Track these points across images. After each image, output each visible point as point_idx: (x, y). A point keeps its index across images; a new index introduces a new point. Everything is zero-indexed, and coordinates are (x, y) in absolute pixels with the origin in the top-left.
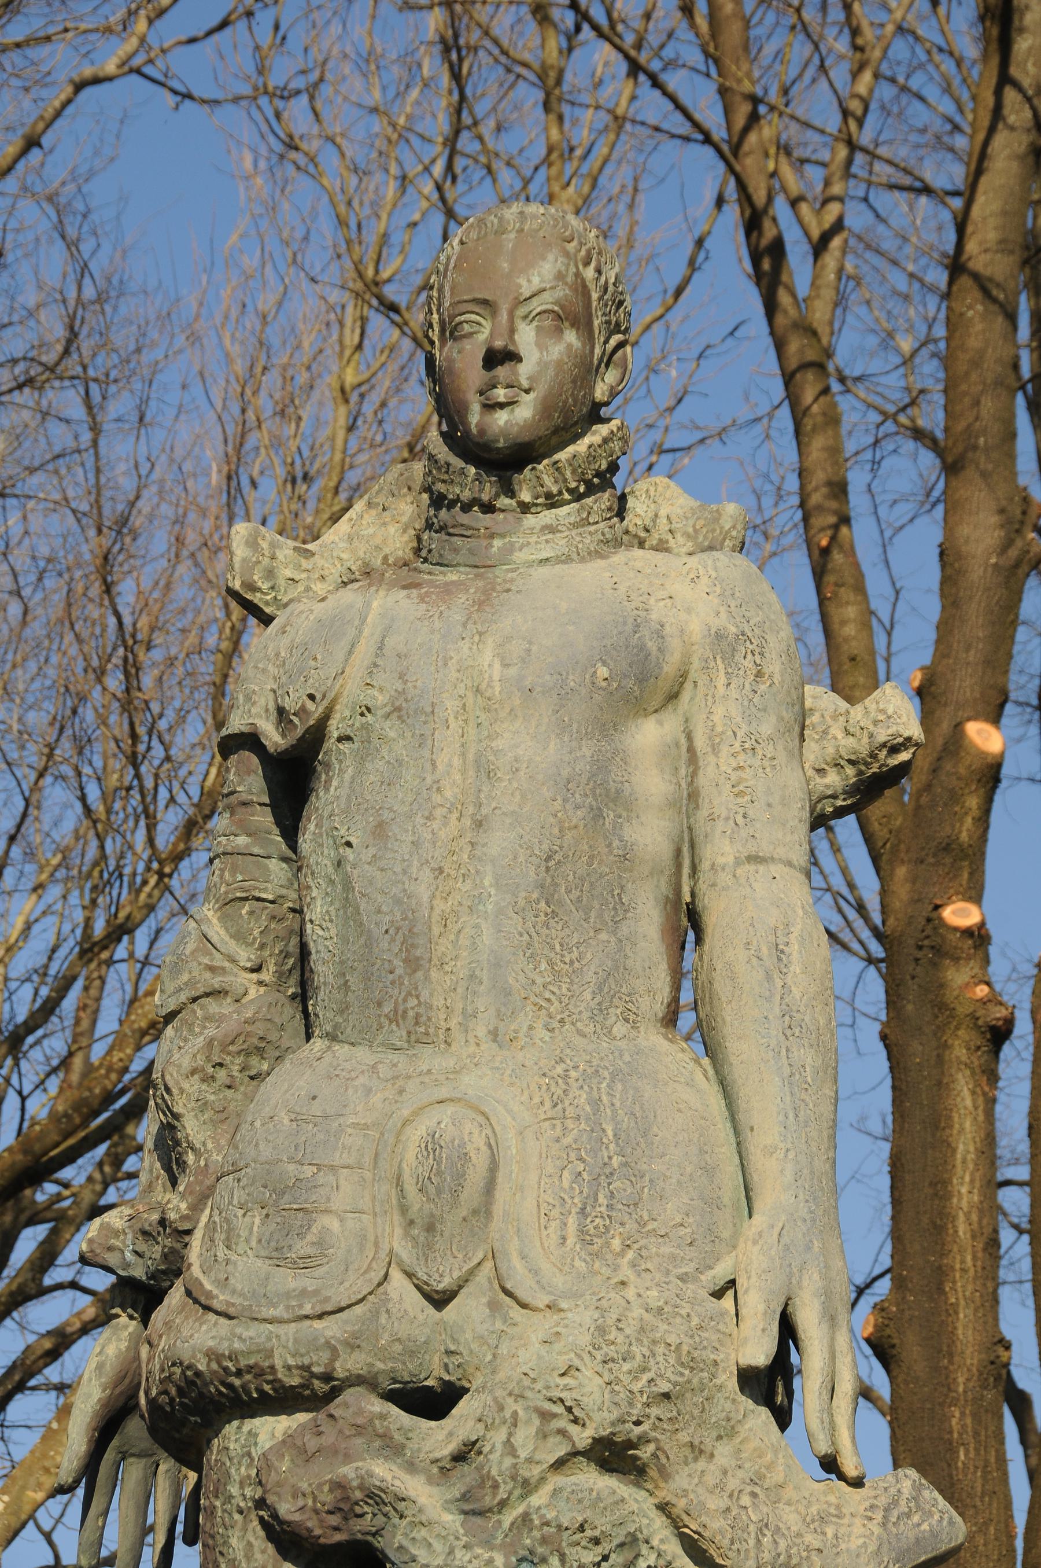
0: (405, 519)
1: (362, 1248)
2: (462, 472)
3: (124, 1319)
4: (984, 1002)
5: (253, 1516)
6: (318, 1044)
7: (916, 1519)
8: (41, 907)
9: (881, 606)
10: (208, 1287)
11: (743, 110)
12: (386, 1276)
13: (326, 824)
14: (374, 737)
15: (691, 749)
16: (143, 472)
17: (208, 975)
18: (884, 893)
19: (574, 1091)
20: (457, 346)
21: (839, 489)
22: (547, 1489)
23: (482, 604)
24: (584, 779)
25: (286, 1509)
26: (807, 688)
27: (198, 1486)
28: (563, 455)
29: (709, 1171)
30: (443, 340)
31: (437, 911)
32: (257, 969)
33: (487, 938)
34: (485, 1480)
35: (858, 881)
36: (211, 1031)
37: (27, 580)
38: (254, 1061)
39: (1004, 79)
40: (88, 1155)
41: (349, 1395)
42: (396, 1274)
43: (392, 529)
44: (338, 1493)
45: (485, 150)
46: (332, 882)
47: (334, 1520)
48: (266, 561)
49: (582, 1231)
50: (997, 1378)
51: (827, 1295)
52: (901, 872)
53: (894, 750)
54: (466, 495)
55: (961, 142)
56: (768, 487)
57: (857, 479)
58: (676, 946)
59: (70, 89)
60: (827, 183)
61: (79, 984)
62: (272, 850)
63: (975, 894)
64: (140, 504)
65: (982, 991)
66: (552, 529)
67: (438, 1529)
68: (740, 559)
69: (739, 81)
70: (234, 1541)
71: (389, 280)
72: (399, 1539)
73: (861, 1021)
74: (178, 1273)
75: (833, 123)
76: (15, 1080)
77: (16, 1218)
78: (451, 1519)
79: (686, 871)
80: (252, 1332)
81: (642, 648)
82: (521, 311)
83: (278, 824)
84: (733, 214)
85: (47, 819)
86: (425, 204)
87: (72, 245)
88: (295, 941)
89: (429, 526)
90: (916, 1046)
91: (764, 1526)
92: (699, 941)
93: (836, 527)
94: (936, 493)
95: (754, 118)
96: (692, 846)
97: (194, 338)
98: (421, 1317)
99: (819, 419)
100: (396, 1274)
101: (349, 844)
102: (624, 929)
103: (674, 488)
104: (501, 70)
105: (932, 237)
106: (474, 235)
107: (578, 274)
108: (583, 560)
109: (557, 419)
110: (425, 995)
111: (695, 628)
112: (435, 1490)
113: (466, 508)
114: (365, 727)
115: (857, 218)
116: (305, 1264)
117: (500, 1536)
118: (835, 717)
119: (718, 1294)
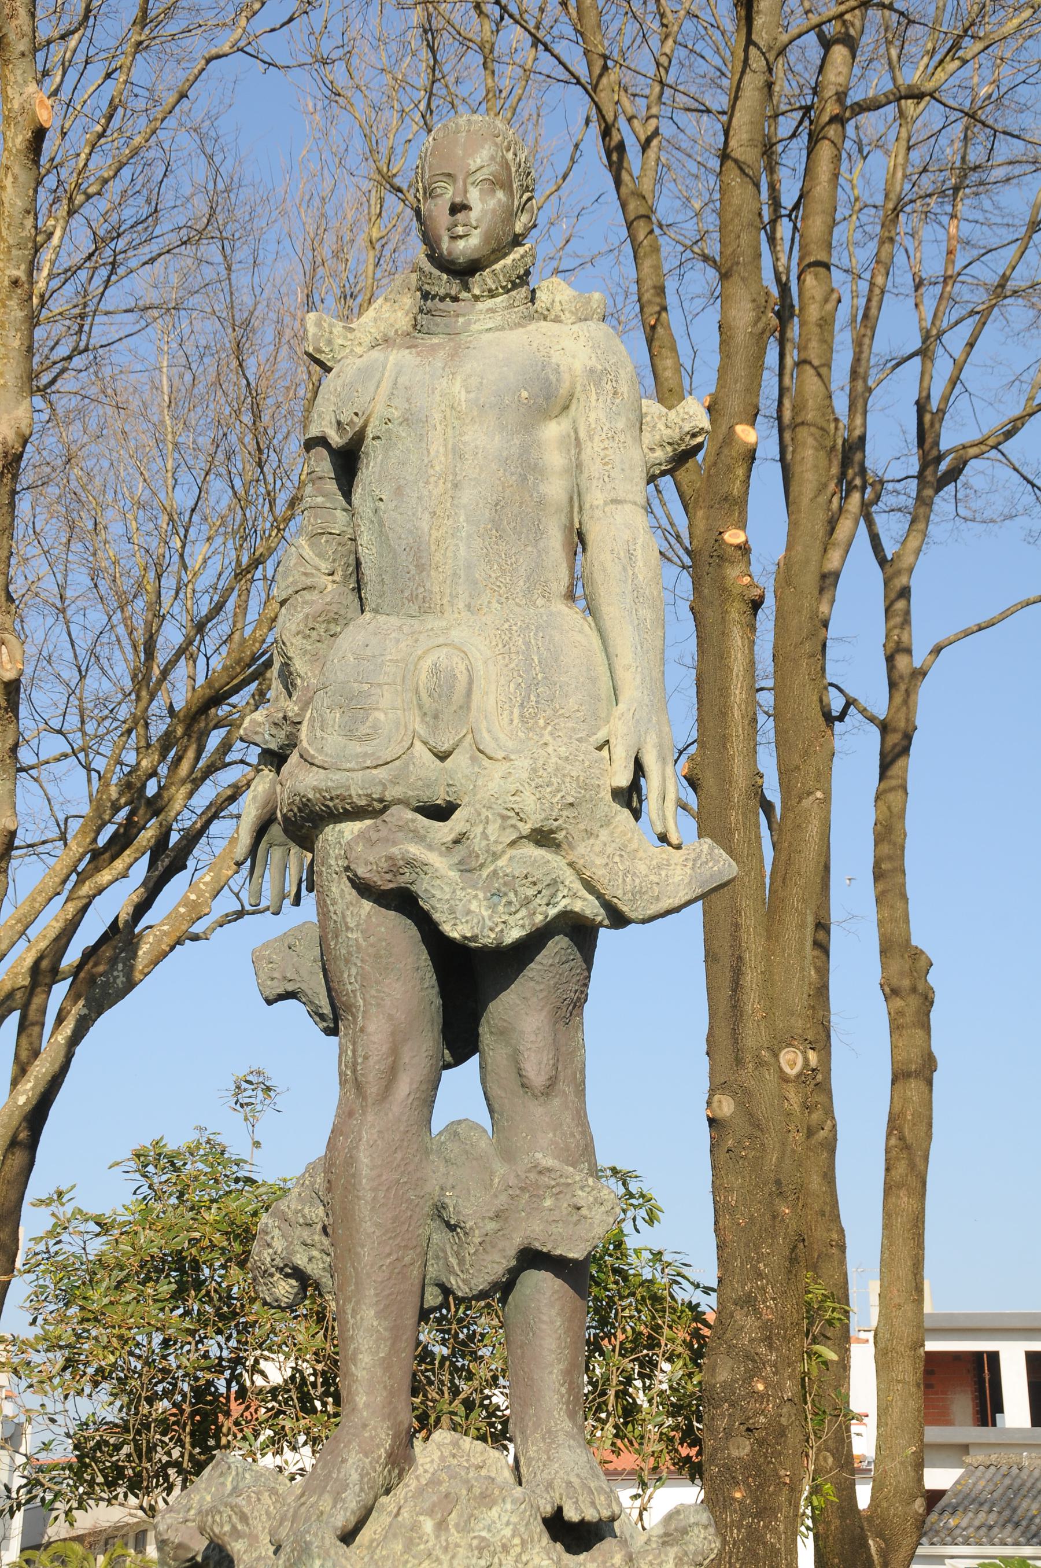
1: (397, 730)
2: (439, 277)
3: (266, 772)
4: (748, 586)
5: (344, 875)
6: (368, 615)
7: (710, 864)
8: (212, 549)
9: (686, 361)
10: (312, 752)
11: (599, 63)
13: (368, 489)
15: (577, 439)
16: (258, 293)
17: (303, 578)
18: (691, 526)
19: (515, 638)
20: (434, 202)
21: (660, 290)
22: (506, 857)
23: (454, 355)
25: (362, 871)
27: (313, 861)
28: (497, 266)
29: (593, 680)
30: (425, 199)
33: (462, 552)
34: (472, 854)
35: (676, 522)
36: (307, 610)
37: (194, 358)
38: (332, 626)
39: (749, 42)
40: (246, 689)
41: (393, 810)
42: (418, 744)
43: (400, 314)
44: (390, 862)
45: (450, 93)
47: (389, 876)
49: (522, 716)
50: (756, 794)
51: (660, 747)
52: (700, 513)
53: (694, 436)
54: (442, 292)
55: (725, 82)
56: (620, 290)
57: (671, 285)
59: (203, 62)
60: (648, 108)
61: (236, 593)
62: (337, 505)
63: (742, 525)
64: (256, 313)
65: (746, 580)
66: (492, 311)
67: (446, 880)
68: (603, 326)
69: (596, 46)
70: (334, 889)
71: (395, 175)
72: (425, 886)
73: (679, 602)
74: (295, 746)
75: (651, 70)
76: (202, 648)
77: (207, 724)
78: (453, 874)
79: (576, 509)
81: (547, 379)
82: (471, 180)
84: (595, 129)
85: (212, 502)
86: (415, 128)
87: (210, 158)
88: (352, 557)
89: (421, 311)
90: (710, 612)
92: (584, 550)
93: (659, 313)
94: (717, 294)
95: (605, 68)
96: (579, 495)
97: (284, 213)
99: (648, 249)
100: (418, 744)
101: (381, 500)
102: (541, 544)
103: (563, 285)
104: (457, 44)
105: (712, 141)
106: (441, 134)
107: (503, 157)
108: (511, 329)
110: (428, 585)
111: (578, 367)
112: (444, 859)
113: (442, 299)
114: (388, 431)
115: (667, 130)
116: (365, 738)
118: (660, 417)
119: (600, 748)
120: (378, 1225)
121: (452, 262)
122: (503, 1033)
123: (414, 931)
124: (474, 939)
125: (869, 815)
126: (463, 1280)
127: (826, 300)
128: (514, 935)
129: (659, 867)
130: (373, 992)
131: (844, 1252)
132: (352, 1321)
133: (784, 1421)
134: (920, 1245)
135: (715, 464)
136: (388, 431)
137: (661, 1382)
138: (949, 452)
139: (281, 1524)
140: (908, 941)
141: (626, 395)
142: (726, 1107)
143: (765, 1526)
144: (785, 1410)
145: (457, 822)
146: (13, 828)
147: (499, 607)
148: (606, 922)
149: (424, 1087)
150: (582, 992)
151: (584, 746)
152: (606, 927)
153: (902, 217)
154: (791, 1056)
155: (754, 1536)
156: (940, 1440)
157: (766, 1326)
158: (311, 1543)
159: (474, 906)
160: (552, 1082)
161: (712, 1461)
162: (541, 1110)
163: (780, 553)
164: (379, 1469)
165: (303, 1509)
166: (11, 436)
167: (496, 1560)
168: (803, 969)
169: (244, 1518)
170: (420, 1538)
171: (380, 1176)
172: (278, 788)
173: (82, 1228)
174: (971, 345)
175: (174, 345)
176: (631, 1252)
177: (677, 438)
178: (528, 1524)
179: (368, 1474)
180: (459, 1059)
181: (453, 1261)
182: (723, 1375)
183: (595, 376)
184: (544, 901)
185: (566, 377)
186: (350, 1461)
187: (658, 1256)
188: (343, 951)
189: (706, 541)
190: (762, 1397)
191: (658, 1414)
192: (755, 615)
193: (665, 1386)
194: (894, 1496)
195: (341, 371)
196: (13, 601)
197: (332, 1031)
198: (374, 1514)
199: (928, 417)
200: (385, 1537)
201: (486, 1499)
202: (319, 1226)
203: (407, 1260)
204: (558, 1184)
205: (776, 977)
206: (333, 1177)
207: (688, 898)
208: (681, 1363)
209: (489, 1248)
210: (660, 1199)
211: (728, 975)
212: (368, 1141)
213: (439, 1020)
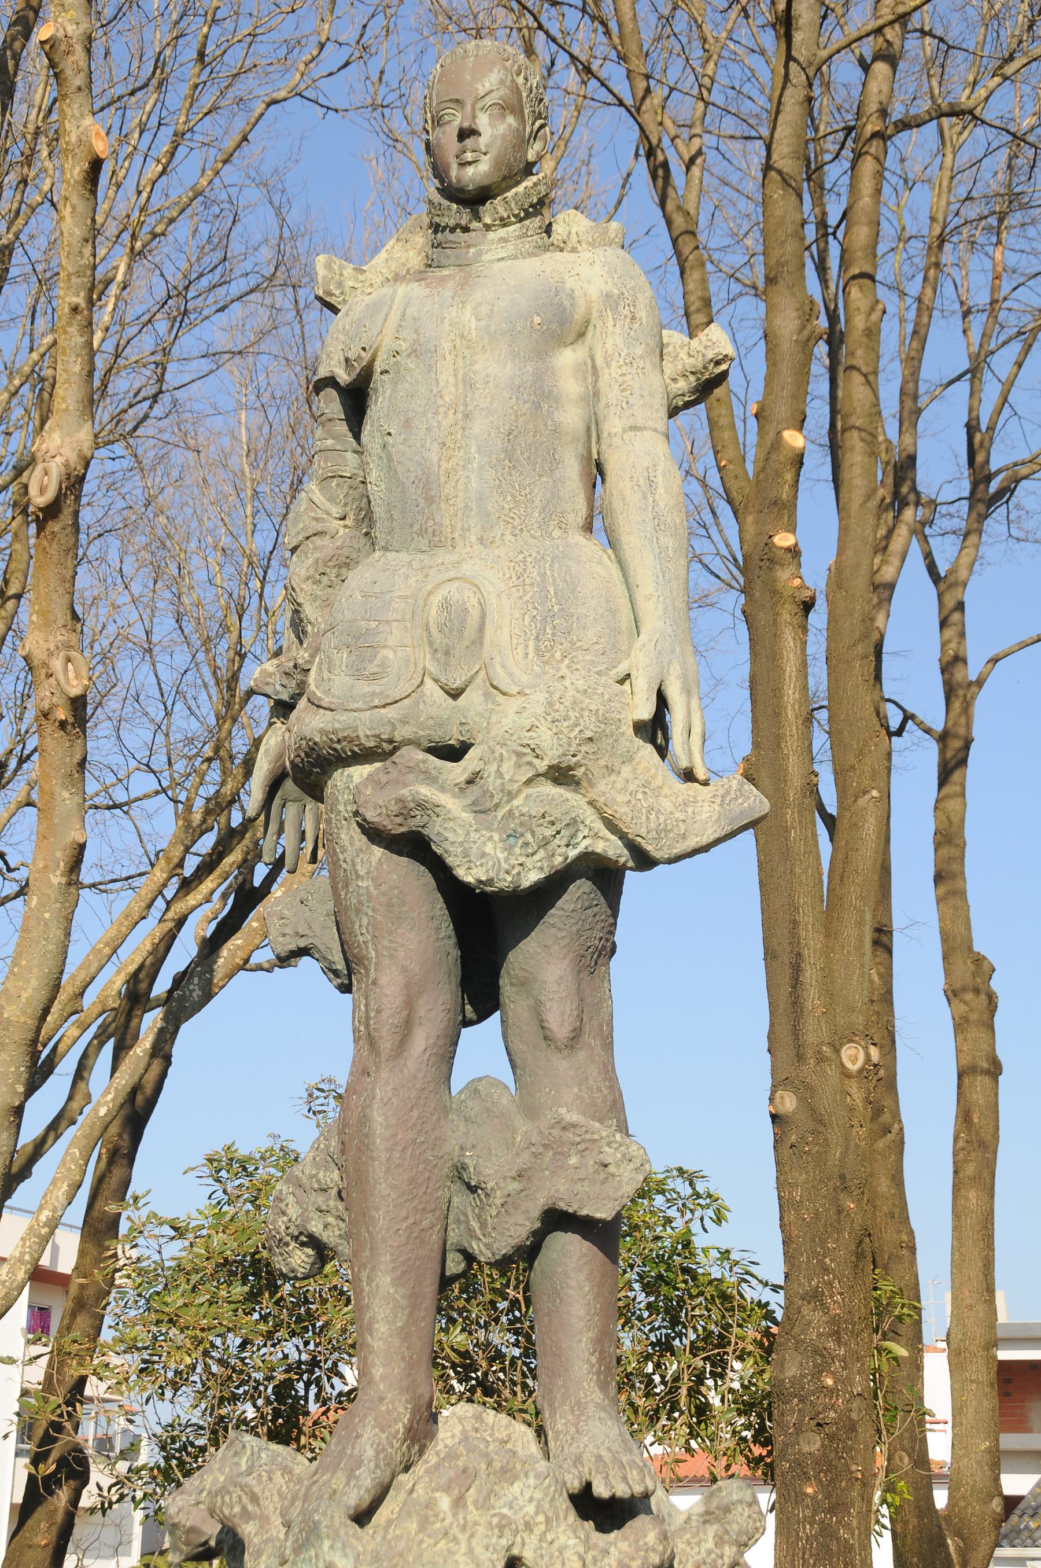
0: (419, 246)
2: (449, 208)
4: (798, 588)
5: (353, 821)
6: (378, 554)
7: (740, 801)
12: (422, 682)
13: (376, 424)
14: (402, 369)
15: (594, 367)
17: (314, 523)
19: (530, 569)
22: (523, 795)
23: (464, 284)
24: (529, 384)
25: (371, 815)
26: (664, 332)
28: (509, 194)
29: (613, 612)
30: (433, 129)
31: (443, 468)
32: (344, 518)
33: (474, 484)
34: (488, 795)
36: (317, 555)
38: (344, 571)
39: (789, 58)
41: (404, 751)
42: (428, 681)
43: (411, 253)
44: (400, 805)
46: (381, 458)
47: (399, 820)
48: (337, 277)
49: (537, 649)
50: (811, 792)
52: (750, 518)
53: (718, 363)
54: (452, 223)
58: (590, 485)
59: (264, 105)
62: (348, 447)
65: (797, 582)
66: (504, 240)
67: (459, 821)
70: (343, 836)
72: (437, 828)
78: (467, 816)
79: (594, 439)
80: (345, 717)
81: (561, 304)
82: (480, 105)
83: (351, 430)
90: (761, 615)
91: (650, 809)
92: (603, 481)
96: (597, 424)
98: (444, 705)
100: (428, 681)
101: (389, 434)
102: (557, 474)
106: (449, 61)
107: (513, 81)
109: (504, 171)
110: (438, 518)
111: (594, 292)
112: (457, 801)
113: (453, 230)
114: (396, 363)
116: (374, 677)
117: (496, 824)
118: (682, 347)
119: (621, 682)
120: (394, 1187)
121: (462, 190)
122: (524, 984)
123: (428, 879)
124: (490, 882)
125: (928, 826)
126: (485, 1245)
127: (873, 309)
128: (532, 877)
129: (685, 804)
130: (386, 943)
131: (914, 1254)
132: (367, 1289)
133: (854, 1416)
134: (990, 1246)
135: (764, 469)
136: (396, 363)
137: (732, 1380)
138: (998, 472)
139: (292, 1503)
140: (970, 948)
141: (644, 321)
142: (789, 1103)
143: (837, 1522)
144: (855, 1405)
145: (471, 761)
146: (82, 841)
147: (513, 539)
148: (631, 864)
149: (441, 1042)
150: (607, 940)
151: (603, 680)
152: (631, 869)
153: (948, 247)
154: (852, 1052)
155: (827, 1532)
156: (1018, 1447)
157: (834, 1321)
158: (319, 1522)
159: (489, 848)
160: (576, 1037)
161: (783, 1456)
162: (565, 1063)
163: (831, 558)
164: (396, 1445)
165: (315, 1488)
166: (73, 458)
167: (518, 1539)
168: (862, 966)
169: (254, 1499)
170: (436, 1516)
171: (395, 1135)
172: (287, 735)
173: (157, 1231)
174: (1019, 365)
175: (253, 397)
176: (699, 1251)
177: (700, 366)
178: (552, 1500)
179: (384, 1450)
180: (483, 1015)
181: (475, 1225)
182: (792, 1371)
183: (611, 301)
184: (564, 842)
185: (581, 303)
186: (366, 1436)
187: (725, 1254)
188: (354, 901)
189: (756, 545)
190: (831, 1392)
191: (729, 1411)
192: (807, 616)
193: (736, 1385)
194: (971, 1495)
195: (350, 309)
196: (79, 620)
197: (346, 988)
198: (391, 1492)
199: (978, 437)
200: (399, 1515)
201: (507, 1474)
202: (334, 1191)
203: (425, 1224)
204: (583, 1141)
205: (836, 974)
206: (346, 1138)
207: (717, 835)
208: (752, 1361)
209: (511, 1210)
210: (727, 1198)
211: (788, 971)
212: (382, 1099)
213: (457, 971)
